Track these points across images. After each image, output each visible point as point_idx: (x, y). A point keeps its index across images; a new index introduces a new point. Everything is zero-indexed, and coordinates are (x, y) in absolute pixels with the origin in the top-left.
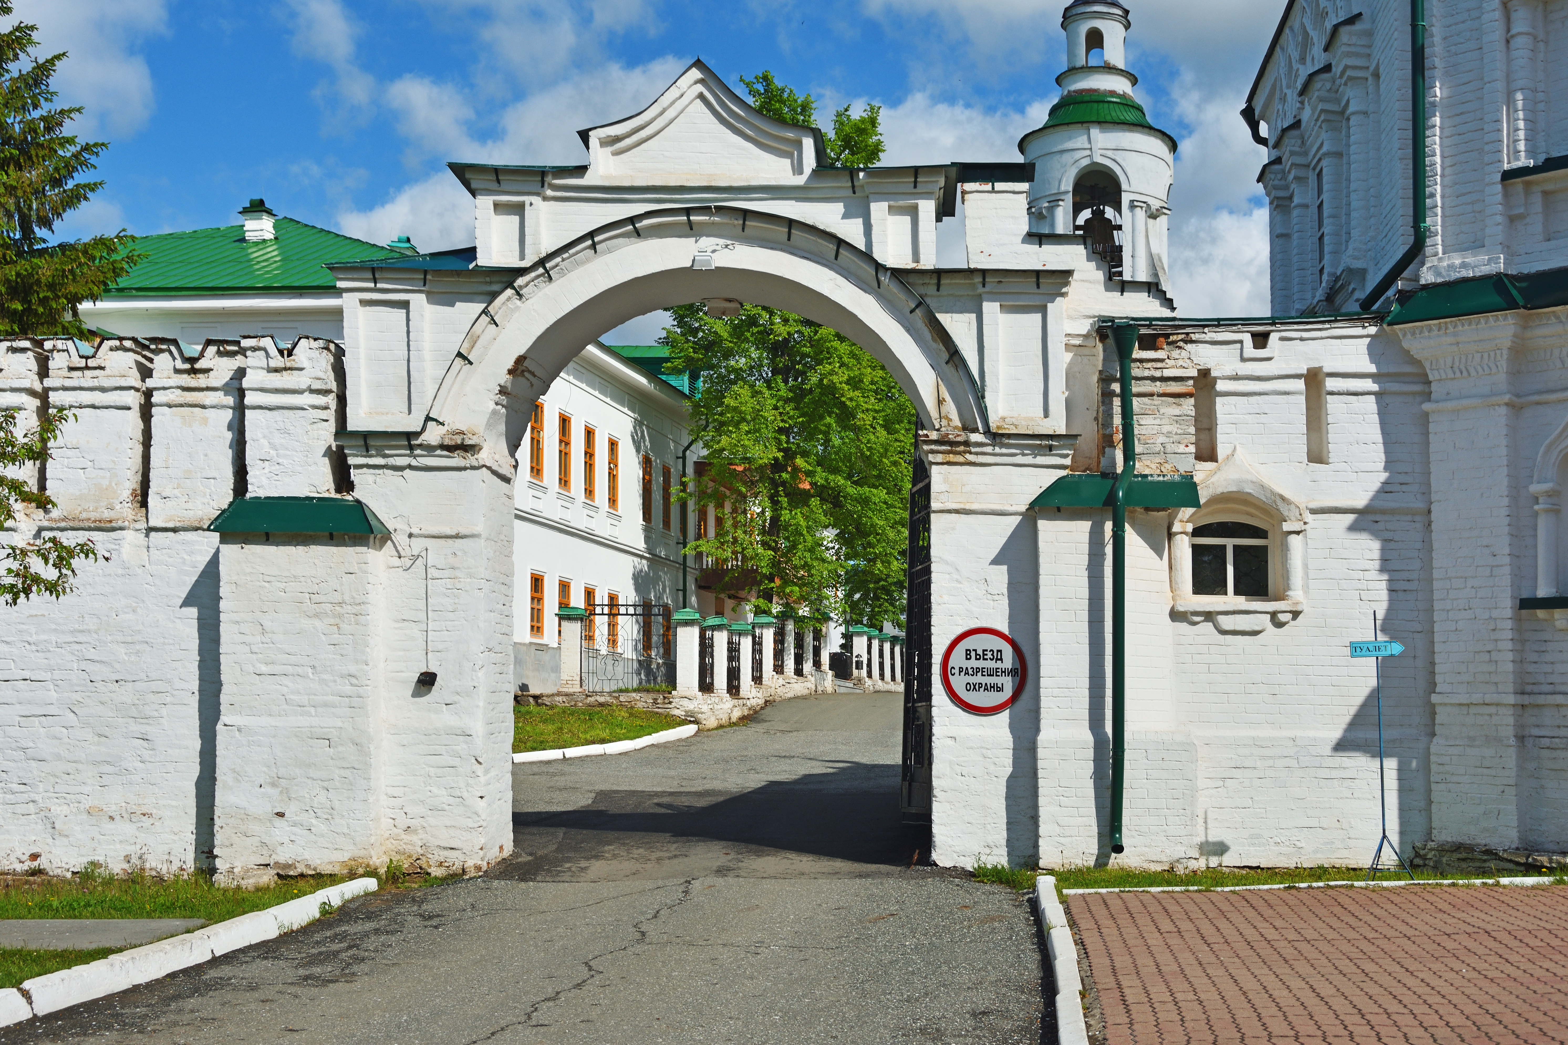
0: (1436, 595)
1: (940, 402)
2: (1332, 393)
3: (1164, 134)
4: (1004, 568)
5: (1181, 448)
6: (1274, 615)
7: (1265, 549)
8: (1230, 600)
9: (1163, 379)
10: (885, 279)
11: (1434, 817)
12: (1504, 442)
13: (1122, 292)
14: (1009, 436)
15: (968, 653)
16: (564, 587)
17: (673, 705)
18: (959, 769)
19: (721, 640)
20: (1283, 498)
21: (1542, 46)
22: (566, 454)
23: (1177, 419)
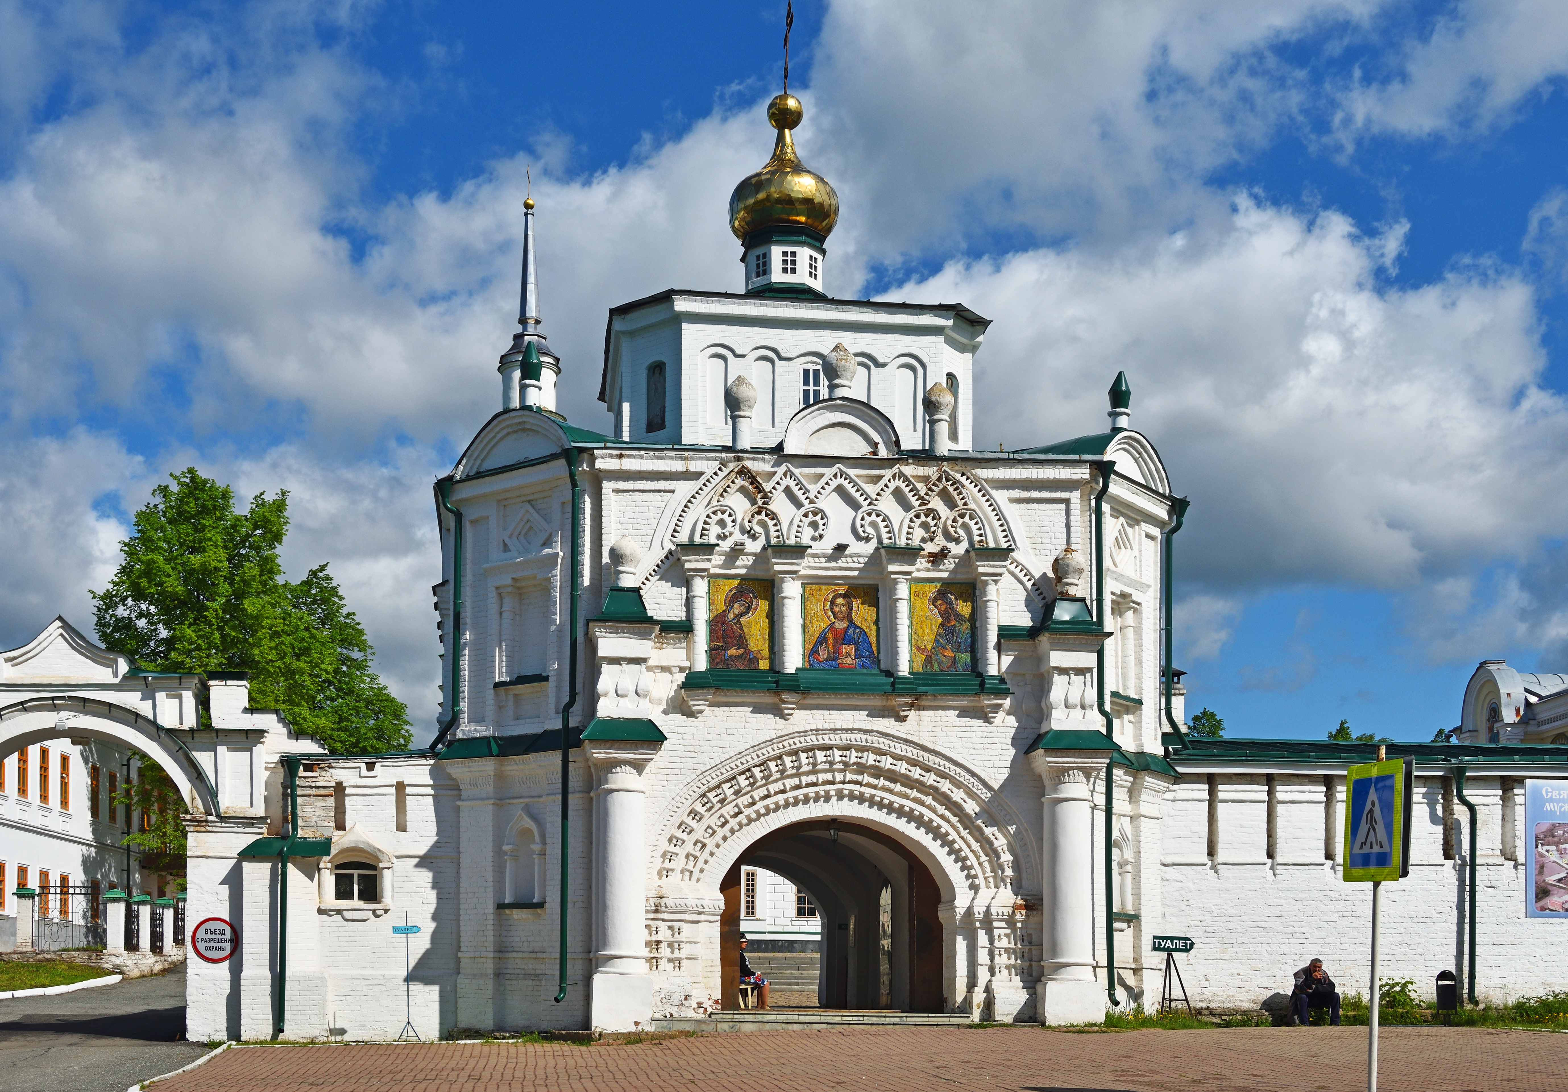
0: (462, 901)
1: (193, 799)
2: (409, 795)
4: (227, 886)
5: (326, 824)
6: (374, 911)
7: (376, 875)
8: (356, 903)
9: (316, 787)
10: (162, 734)
11: (459, 1015)
12: (491, 824)
13: (297, 739)
14: (230, 817)
15: (206, 931)
16: (22, 871)
17: (104, 960)
18: (201, 991)
19: (145, 913)
20: (380, 850)
21: (518, 617)
22: (24, 769)
23: (324, 809)
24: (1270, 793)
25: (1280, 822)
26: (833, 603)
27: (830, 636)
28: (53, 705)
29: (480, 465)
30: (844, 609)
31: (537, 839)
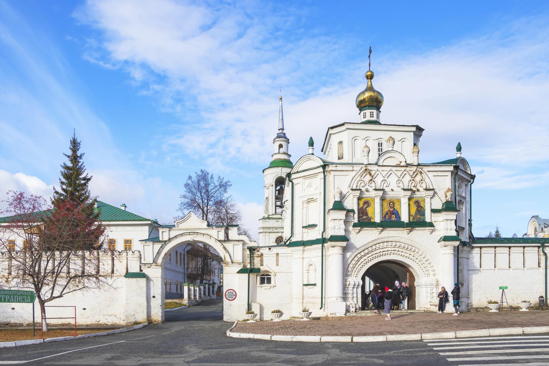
7: (271, 278)
10: (217, 241)
15: (228, 292)
26: (389, 204)
28: (189, 234)
29: (298, 170)
30: (392, 205)
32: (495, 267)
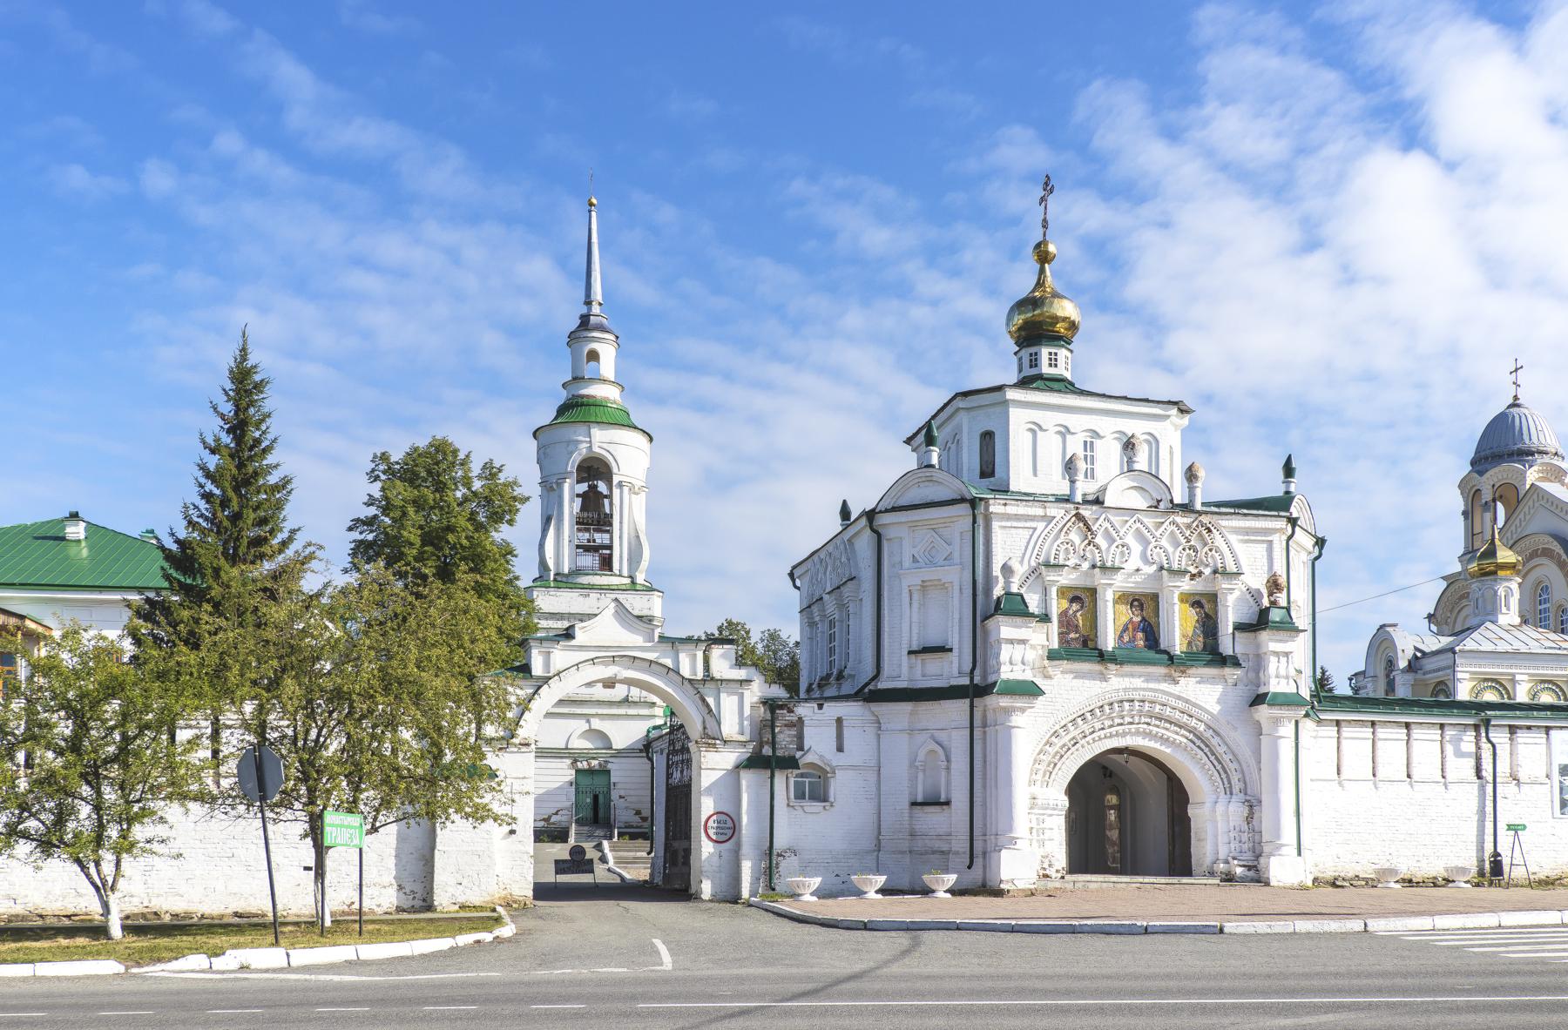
3: (644, 432)
10: (686, 683)
23: (789, 736)
24: (1408, 735)
25: (1379, 753)
27: (1130, 626)
31: (943, 758)
32: (1374, 775)
